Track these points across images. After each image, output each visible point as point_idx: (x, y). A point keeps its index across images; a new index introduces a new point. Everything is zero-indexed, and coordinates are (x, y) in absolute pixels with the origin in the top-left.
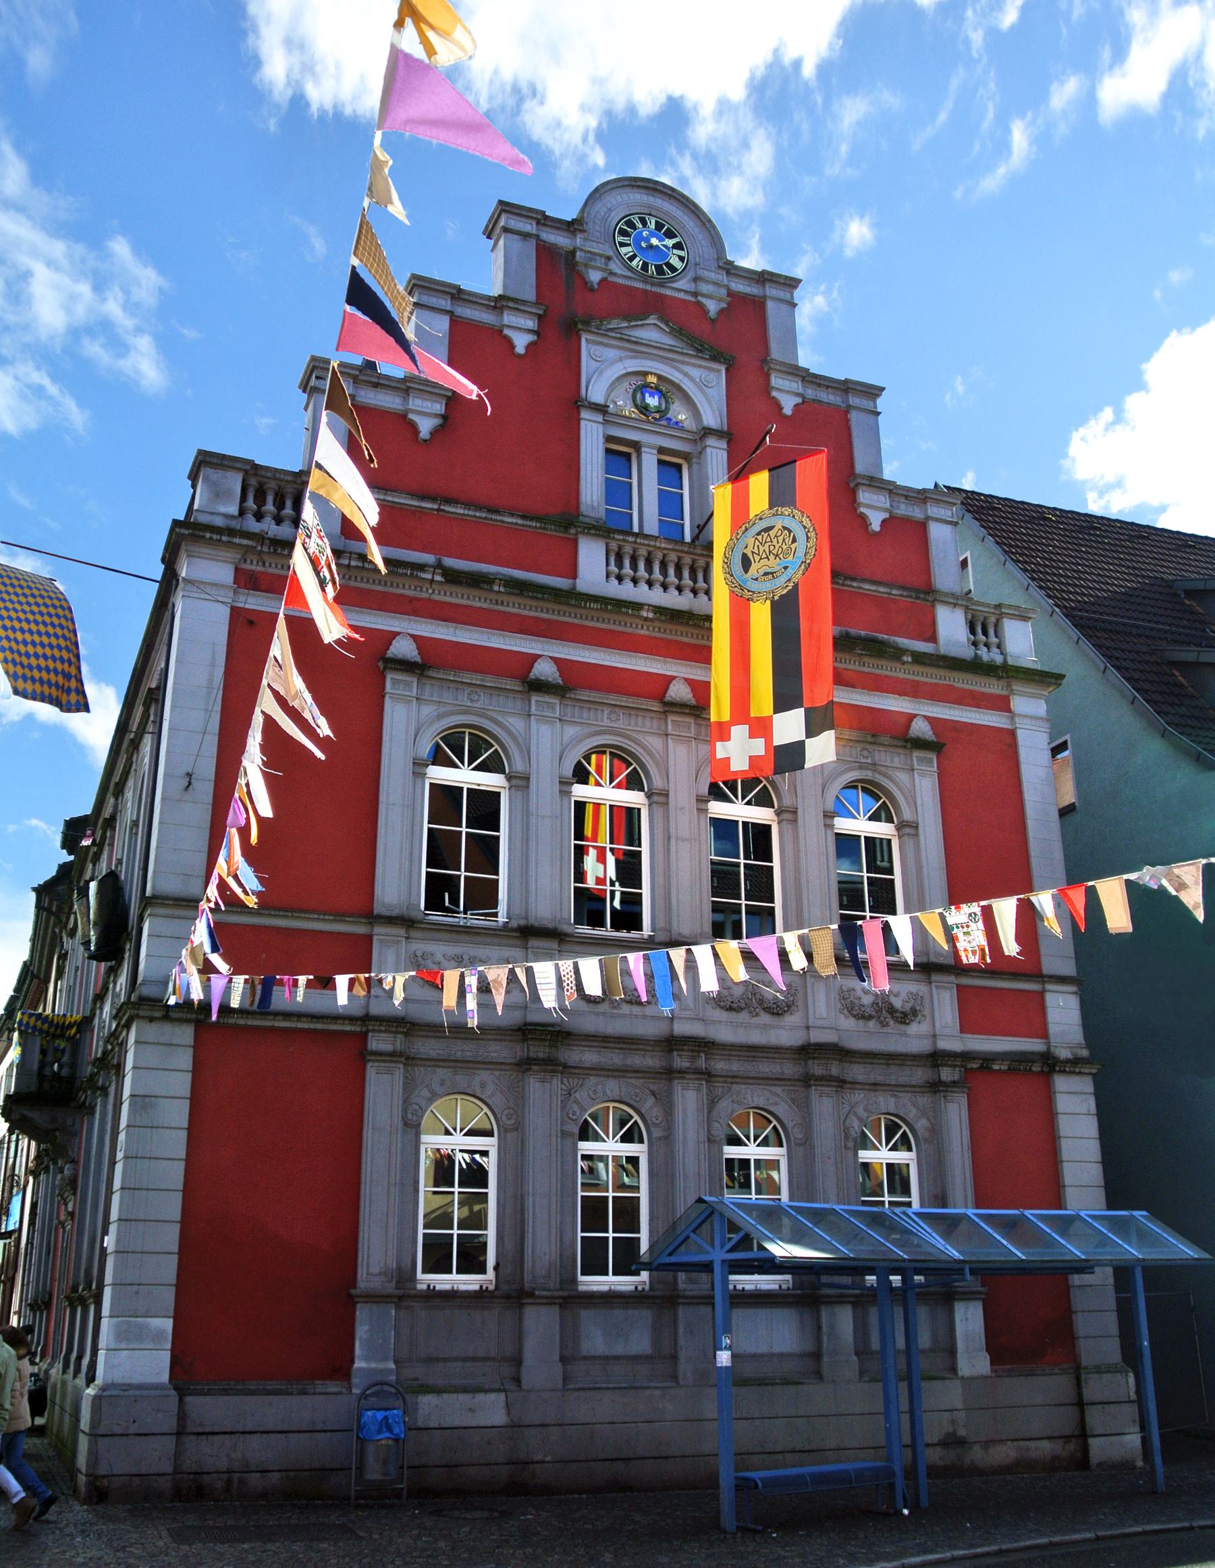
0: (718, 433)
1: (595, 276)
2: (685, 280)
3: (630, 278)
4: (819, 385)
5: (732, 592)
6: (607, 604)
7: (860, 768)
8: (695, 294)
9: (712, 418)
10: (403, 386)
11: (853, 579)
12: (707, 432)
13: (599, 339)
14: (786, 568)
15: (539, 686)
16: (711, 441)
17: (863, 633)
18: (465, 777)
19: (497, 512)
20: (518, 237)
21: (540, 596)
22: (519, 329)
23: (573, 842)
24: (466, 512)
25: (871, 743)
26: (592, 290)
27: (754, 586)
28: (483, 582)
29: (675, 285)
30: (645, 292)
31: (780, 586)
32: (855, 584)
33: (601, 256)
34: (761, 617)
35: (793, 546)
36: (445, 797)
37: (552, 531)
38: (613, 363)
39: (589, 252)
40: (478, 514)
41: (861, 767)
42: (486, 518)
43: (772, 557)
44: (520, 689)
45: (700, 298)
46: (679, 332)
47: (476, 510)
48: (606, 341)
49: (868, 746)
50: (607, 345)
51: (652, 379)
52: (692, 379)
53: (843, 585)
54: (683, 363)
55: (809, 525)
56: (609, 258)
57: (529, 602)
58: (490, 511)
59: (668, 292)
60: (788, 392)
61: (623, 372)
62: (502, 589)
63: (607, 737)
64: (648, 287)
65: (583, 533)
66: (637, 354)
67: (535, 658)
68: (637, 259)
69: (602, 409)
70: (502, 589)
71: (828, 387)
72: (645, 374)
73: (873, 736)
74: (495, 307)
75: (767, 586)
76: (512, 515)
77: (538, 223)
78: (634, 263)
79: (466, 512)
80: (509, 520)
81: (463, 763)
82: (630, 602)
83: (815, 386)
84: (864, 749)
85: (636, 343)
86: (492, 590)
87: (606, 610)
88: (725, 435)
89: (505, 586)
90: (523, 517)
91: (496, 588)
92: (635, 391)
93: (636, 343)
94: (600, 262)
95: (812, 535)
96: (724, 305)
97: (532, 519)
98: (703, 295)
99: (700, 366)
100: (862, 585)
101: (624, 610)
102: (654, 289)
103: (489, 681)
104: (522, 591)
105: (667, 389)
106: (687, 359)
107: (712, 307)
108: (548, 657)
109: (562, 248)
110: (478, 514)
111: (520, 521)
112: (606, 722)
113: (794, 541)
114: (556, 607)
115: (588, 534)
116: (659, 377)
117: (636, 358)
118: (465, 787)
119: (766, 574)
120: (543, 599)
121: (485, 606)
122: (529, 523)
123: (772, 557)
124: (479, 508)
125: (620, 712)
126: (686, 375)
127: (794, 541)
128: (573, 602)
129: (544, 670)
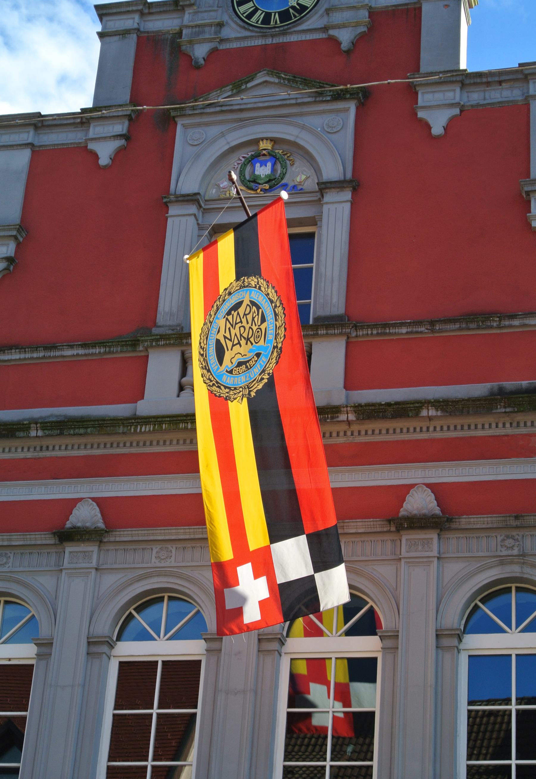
0: (338, 185)
1: (200, 52)
2: (316, 17)
3: (246, 38)
4: (488, 84)
5: (211, 392)
6: (160, 423)
7: (502, 563)
8: (325, 29)
9: (332, 171)
10: (520, 76)
11: (513, 317)
12: (325, 187)
13: (197, 120)
14: (258, 355)
15: (67, 536)
16: (330, 197)
17: (525, 383)
18: (163, 649)
19: (53, 347)
20: (116, 38)
21: (82, 431)
22: (104, 138)
23: (198, 711)
24: (22, 356)
25: (517, 527)
26: (198, 67)
27: (228, 380)
28: (19, 430)
29: (304, 27)
30: (264, 47)
31: (254, 378)
32: (516, 322)
33: (210, 25)
34: (239, 413)
35: (263, 327)
36: (135, 678)
37: (119, 353)
38: (215, 140)
39: (197, 26)
40: (35, 355)
41: (502, 562)
42: (44, 357)
43: (243, 342)
44: (52, 542)
45: (331, 32)
46: (299, 78)
47: (32, 352)
48: (205, 119)
49: (514, 533)
50: (207, 124)
51: (265, 145)
52: (311, 131)
53: (499, 327)
54: (301, 115)
55: (275, 298)
56: (220, 25)
57: (76, 440)
58: (46, 348)
59: (294, 38)
60: (438, 106)
61: (227, 147)
62: (40, 433)
63: (155, 580)
64: (269, 41)
65: (152, 346)
66: (243, 122)
67: (73, 503)
68: (259, 12)
69: (192, 199)
70: (40, 433)
71: (500, 83)
72: (256, 142)
73: (517, 518)
74: (82, 123)
75: (241, 380)
76: (71, 347)
77: (142, 14)
78: (254, 19)
79: (22, 356)
80: (68, 352)
81: (510, 628)
82: (156, 417)
83: (482, 88)
84: (508, 537)
85: (241, 110)
86: (28, 437)
87: (161, 430)
88: (354, 184)
89: (43, 429)
90: (84, 346)
91: (33, 433)
92: (245, 165)
93: (241, 110)
94: (209, 33)
95: (279, 310)
96: (364, 29)
97: (94, 346)
98: (334, 27)
99: (324, 112)
100: (527, 321)
101: (182, 426)
102: (276, 40)
103: (17, 539)
104: (62, 430)
105: (282, 153)
106: (306, 109)
107: (345, 37)
108: (84, 498)
109: (168, 32)
110: (35, 355)
111: (81, 351)
112: (155, 562)
113: (263, 320)
114: (108, 439)
115: (158, 346)
116: (274, 141)
117: (241, 128)
118: (160, 660)
119: (240, 364)
120: (86, 434)
121: (29, 455)
122: (91, 351)
123: (243, 342)
124: (35, 348)
125: (188, 545)
126: (303, 127)
127: (263, 320)
128: (121, 430)
129: (86, 515)
